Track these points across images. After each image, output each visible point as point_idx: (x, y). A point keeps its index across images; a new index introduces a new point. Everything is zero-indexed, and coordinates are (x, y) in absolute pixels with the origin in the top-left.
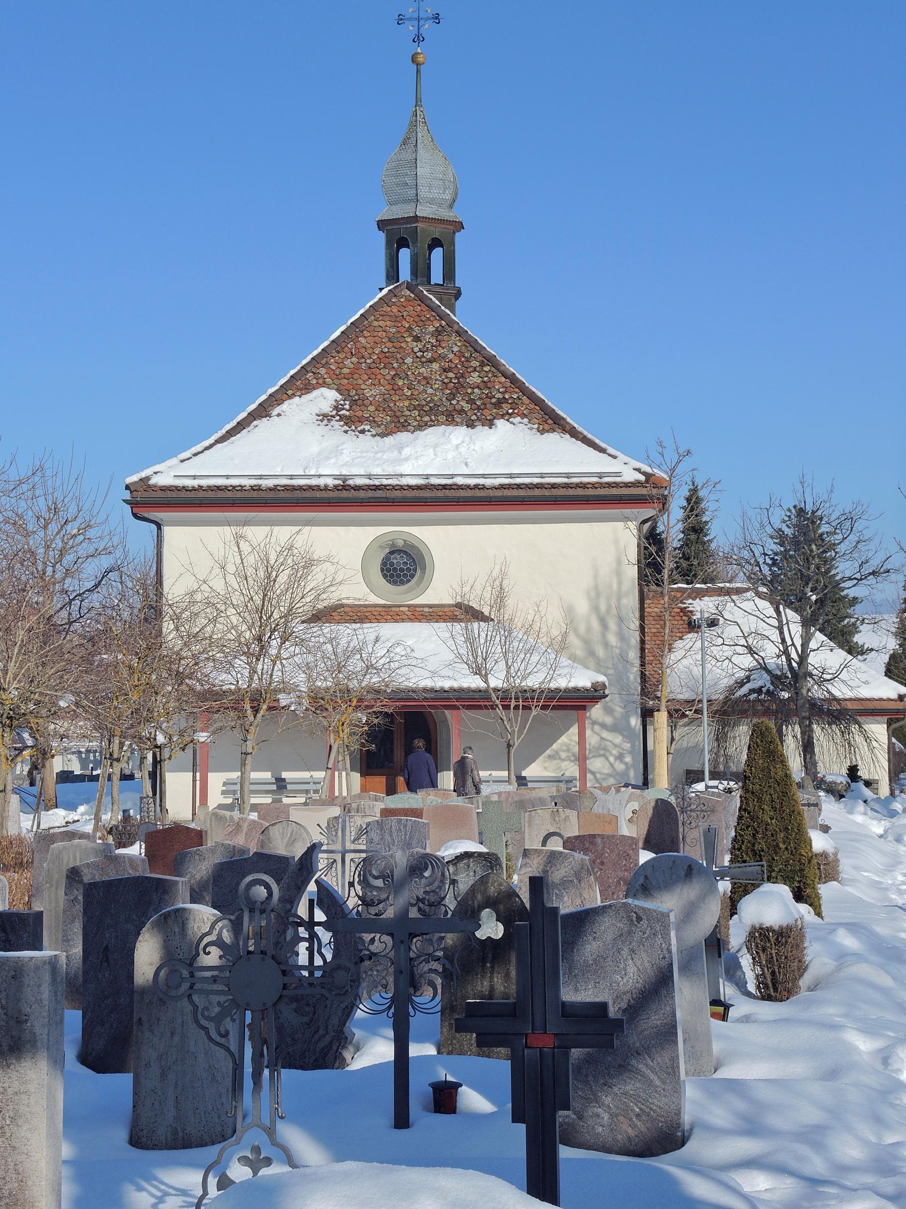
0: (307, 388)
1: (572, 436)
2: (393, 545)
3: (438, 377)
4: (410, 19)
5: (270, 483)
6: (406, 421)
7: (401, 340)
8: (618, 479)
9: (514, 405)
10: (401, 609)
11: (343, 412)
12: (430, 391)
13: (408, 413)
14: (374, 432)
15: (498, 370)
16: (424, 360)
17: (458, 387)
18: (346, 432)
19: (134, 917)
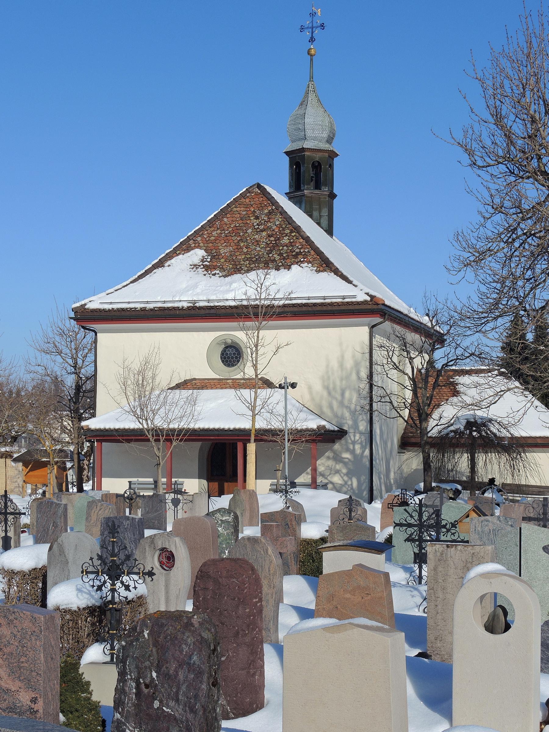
0: (188, 249)
1: (335, 274)
2: (225, 343)
3: (264, 240)
4: (308, 28)
5: (151, 306)
6: (240, 267)
7: (248, 218)
8: (354, 300)
9: (305, 256)
10: (228, 381)
11: (206, 263)
12: (258, 249)
13: (243, 262)
14: (221, 274)
15: (299, 234)
16: (258, 230)
17: (274, 246)
18: (205, 275)
19: (227, 552)
